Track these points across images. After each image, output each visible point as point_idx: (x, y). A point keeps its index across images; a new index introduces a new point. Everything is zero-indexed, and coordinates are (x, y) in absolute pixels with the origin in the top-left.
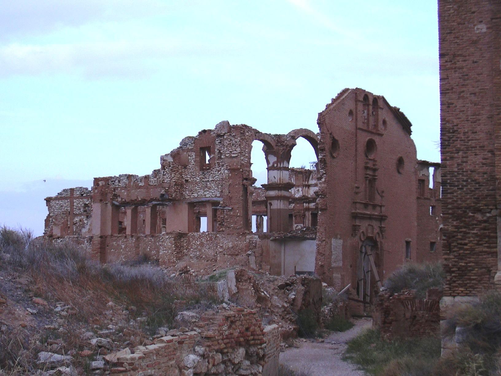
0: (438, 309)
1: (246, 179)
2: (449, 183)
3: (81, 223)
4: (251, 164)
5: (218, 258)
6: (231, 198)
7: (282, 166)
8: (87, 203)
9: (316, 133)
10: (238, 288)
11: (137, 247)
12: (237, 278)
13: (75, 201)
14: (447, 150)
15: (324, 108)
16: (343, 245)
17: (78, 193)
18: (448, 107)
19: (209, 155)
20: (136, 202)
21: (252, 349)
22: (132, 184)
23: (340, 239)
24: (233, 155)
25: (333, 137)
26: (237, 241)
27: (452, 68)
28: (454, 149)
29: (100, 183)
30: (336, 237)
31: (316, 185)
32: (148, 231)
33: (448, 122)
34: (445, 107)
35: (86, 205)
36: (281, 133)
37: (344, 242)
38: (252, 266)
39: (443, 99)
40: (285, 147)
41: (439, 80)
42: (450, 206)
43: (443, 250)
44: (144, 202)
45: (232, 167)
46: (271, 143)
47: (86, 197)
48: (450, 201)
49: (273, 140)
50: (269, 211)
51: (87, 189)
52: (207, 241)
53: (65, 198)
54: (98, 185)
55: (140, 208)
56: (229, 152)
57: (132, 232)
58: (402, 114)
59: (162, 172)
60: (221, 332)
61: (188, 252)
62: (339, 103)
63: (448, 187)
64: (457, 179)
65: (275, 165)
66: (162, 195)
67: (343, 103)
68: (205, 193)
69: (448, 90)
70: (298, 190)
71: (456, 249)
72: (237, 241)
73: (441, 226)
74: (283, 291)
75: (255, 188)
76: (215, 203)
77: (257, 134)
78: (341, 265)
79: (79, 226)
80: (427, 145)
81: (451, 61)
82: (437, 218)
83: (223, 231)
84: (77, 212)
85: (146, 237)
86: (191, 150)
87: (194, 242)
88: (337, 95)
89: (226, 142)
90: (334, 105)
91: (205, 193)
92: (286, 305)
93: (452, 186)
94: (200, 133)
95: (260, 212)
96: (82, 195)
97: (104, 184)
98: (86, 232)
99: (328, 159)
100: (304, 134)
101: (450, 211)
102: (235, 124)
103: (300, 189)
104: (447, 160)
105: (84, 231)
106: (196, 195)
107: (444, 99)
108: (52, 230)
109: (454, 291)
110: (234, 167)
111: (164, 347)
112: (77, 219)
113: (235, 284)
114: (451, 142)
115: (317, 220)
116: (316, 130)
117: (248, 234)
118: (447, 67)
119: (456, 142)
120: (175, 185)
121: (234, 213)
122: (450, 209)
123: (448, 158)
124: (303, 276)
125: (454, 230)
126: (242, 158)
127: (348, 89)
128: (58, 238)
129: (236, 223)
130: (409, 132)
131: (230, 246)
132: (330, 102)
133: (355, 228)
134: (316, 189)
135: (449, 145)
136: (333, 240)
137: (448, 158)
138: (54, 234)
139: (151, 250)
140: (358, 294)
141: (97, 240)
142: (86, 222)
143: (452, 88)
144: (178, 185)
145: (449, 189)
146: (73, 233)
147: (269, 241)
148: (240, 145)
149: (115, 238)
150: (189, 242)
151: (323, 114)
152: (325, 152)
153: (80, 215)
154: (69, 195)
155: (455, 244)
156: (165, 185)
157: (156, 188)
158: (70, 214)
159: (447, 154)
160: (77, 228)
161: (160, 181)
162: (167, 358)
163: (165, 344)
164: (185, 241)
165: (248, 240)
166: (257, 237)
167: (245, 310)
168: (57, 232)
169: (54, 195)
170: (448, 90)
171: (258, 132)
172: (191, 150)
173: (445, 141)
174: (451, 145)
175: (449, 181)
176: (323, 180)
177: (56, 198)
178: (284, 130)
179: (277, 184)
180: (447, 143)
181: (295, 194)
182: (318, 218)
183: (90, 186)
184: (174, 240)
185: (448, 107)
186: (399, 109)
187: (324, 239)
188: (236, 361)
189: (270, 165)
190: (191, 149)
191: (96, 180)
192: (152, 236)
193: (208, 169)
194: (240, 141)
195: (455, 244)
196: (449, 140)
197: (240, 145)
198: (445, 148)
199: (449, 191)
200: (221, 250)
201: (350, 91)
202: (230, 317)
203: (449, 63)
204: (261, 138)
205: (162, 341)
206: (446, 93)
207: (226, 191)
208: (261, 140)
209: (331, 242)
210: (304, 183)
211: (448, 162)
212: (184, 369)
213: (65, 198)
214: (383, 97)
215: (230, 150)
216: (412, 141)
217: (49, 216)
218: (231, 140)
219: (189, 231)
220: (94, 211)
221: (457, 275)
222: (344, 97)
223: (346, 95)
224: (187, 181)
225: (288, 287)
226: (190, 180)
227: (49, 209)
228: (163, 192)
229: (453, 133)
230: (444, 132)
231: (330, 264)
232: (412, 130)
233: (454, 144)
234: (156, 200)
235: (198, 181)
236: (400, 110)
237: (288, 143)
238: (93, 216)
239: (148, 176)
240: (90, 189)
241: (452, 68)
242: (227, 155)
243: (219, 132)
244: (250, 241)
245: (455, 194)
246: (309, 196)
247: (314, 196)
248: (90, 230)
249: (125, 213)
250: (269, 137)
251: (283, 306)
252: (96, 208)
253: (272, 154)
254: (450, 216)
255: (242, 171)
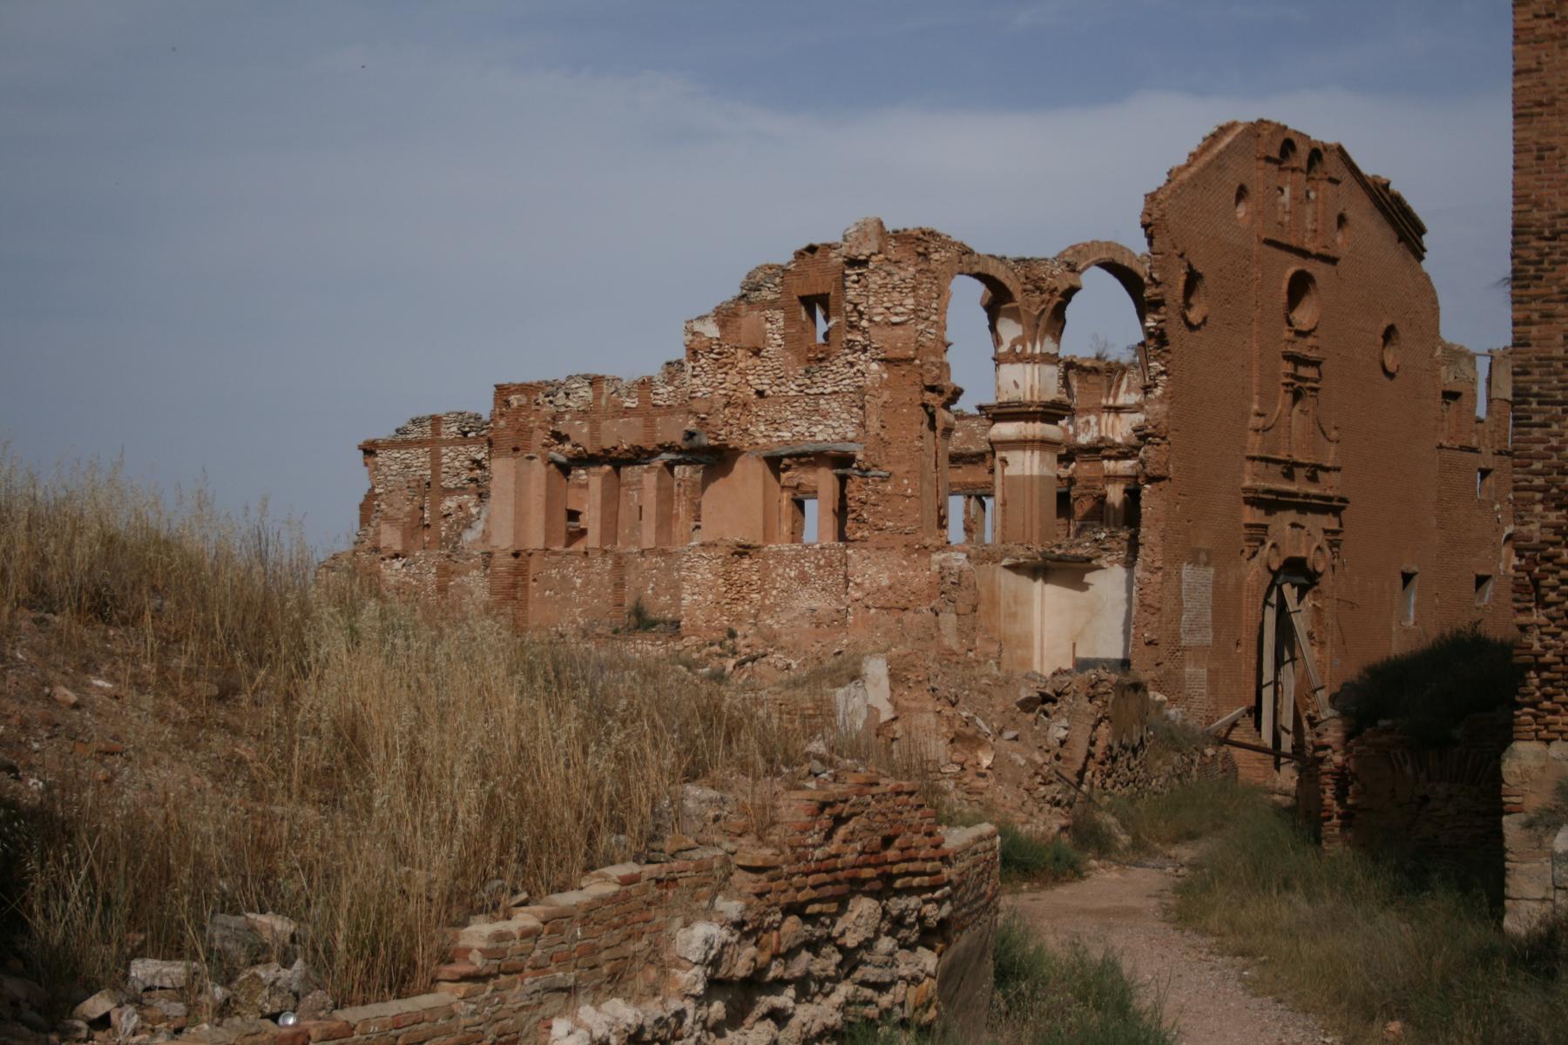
0: (1497, 779)
1: (932, 389)
2: (1536, 395)
3: (461, 514)
4: (947, 346)
5: (850, 618)
6: (887, 444)
7: (1037, 350)
8: (479, 457)
9: (1138, 254)
10: (896, 706)
11: (619, 585)
12: (893, 676)
13: (444, 451)
14: (1532, 291)
15: (1162, 180)
16: (1216, 583)
17: (454, 429)
18: (1540, 158)
19: (827, 318)
20: (614, 454)
21: (896, 905)
22: (603, 402)
23: (1207, 564)
24: (895, 319)
25: (1190, 266)
26: (904, 568)
27: (1553, 37)
28: (1555, 289)
29: (514, 400)
30: (1195, 561)
31: (1137, 408)
32: (648, 538)
33: (1537, 204)
34: (1529, 160)
35: (478, 464)
36: (1038, 255)
37: (1217, 575)
38: (946, 642)
39: (1520, 135)
40: (1046, 296)
41: (1511, 119)
42: (1537, 466)
43: (1515, 600)
44: (639, 456)
45: (890, 355)
46: (1007, 283)
47: (475, 441)
48: (1540, 447)
49: (1011, 275)
50: (998, 482)
51: (478, 418)
52: (818, 567)
53: (420, 443)
54: (507, 403)
55: (628, 473)
56: (882, 310)
57: (602, 540)
58: (1397, 199)
59: (689, 366)
60: (800, 850)
61: (764, 598)
62: (1209, 165)
63: (1534, 406)
64: (1560, 381)
65: (1019, 349)
66: (691, 435)
67: (1218, 164)
68: (814, 429)
69: (1540, 104)
70: (1088, 422)
71: (1552, 596)
72: (904, 568)
73: (1509, 530)
74: (1031, 717)
75: (960, 416)
76: (842, 461)
77: (965, 258)
78: (1209, 640)
79: (457, 522)
80: (1472, 303)
81: (1551, 15)
82: (1497, 506)
83: (864, 540)
84: (449, 483)
85: (642, 553)
86: (772, 304)
87: (780, 571)
88: (1200, 141)
89: (875, 280)
90: (1192, 170)
91: (814, 429)
92: (1038, 758)
93: (1546, 403)
94: (800, 255)
95: (974, 486)
96: (465, 434)
97: (524, 401)
98: (475, 541)
99: (1176, 331)
100: (1105, 256)
101: (1539, 481)
102: (900, 228)
103: (1093, 419)
104: (1532, 323)
105: (469, 536)
106: (787, 435)
107: (1527, 134)
108: (378, 533)
109: (1546, 726)
110: (897, 353)
111: (613, 899)
112: (450, 503)
113: (888, 694)
114: (1546, 265)
115: (1139, 507)
116: (1136, 244)
117: (938, 549)
118: (1538, 32)
119: (1559, 268)
120: (727, 405)
121: (894, 487)
122: (1537, 473)
123: (1535, 316)
124: (1091, 674)
125: (1551, 537)
126: (921, 327)
127: (1233, 125)
128: (397, 556)
129: (902, 516)
130: (1418, 252)
131: (885, 582)
132: (1183, 161)
133: (1258, 534)
134: (1138, 418)
135: (1540, 278)
136: (1186, 570)
137: (1535, 316)
138: (382, 545)
139: (656, 595)
140: (1258, 726)
141: (503, 562)
142: (474, 511)
143: (1552, 102)
144: (736, 405)
145: (1536, 412)
146: (440, 542)
147: (998, 568)
148: (914, 289)
149: (554, 559)
150: (765, 573)
151: (1161, 196)
152: (1163, 309)
153: (461, 490)
154: (426, 433)
155: (1551, 580)
156: (696, 405)
157: (672, 414)
158: (429, 488)
159: (1533, 305)
160: (450, 528)
161: (684, 394)
162: (618, 935)
163: (615, 888)
164: (755, 567)
165: (936, 568)
166: (963, 556)
167: (882, 781)
168: (391, 538)
169: (384, 432)
170: (1540, 104)
171: (970, 252)
172: (772, 304)
173: (1528, 263)
174: (1546, 275)
175: (1535, 389)
176: (1158, 391)
177: (391, 445)
178: (1045, 245)
179: (1021, 404)
180: (1532, 270)
181: (1076, 435)
182: (1143, 503)
183: (484, 407)
184: (723, 565)
185: (1540, 158)
186: (1386, 186)
187: (1158, 564)
188: (851, 941)
189: (1004, 349)
190: (773, 302)
191: (502, 391)
192: (663, 553)
193: (821, 360)
194: (914, 278)
195: (1551, 580)
196: (1541, 262)
197: (914, 289)
198: (1528, 287)
199: (1536, 419)
200: (858, 595)
201: (1239, 129)
202: (831, 805)
203: (1544, 23)
204: (977, 269)
205: (606, 879)
206: (1532, 115)
207: (874, 424)
208: (978, 276)
209: (1179, 573)
210: (1104, 402)
211: (1534, 330)
212: (678, 966)
213: (420, 443)
214: (1340, 150)
215: (882, 301)
216: (1427, 277)
217: (371, 496)
218: (889, 274)
219: (768, 536)
220: (495, 479)
221: (1559, 676)
222: (1221, 146)
223: (1227, 139)
224: (760, 394)
225: (1047, 707)
226: (769, 392)
227: (370, 473)
228: (691, 425)
229: (1553, 239)
230: (1525, 207)
231: (1176, 637)
232: (1426, 245)
233: (1555, 275)
234: (668, 449)
235: (792, 393)
236: (1391, 187)
237: (1057, 283)
238: (493, 493)
239: (650, 379)
240: (486, 417)
241: (1553, 37)
242: (877, 319)
243: (854, 252)
244: (942, 568)
245: (1555, 428)
246: (1119, 440)
247: (1134, 441)
248: (486, 536)
249: (586, 486)
250: (1002, 268)
251: (1031, 762)
252: (502, 469)
253: (1009, 317)
254: (1539, 496)
255: (921, 366)
